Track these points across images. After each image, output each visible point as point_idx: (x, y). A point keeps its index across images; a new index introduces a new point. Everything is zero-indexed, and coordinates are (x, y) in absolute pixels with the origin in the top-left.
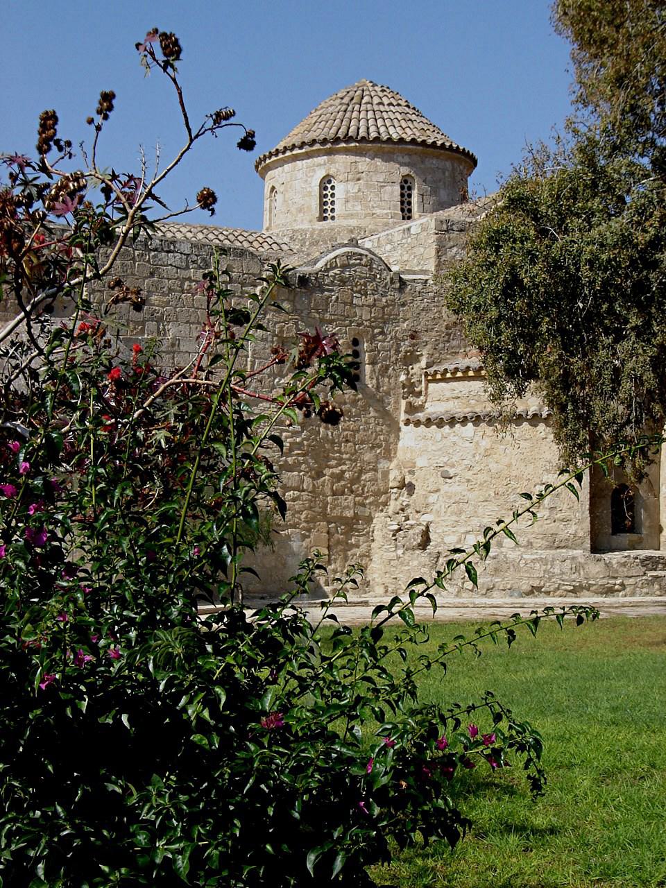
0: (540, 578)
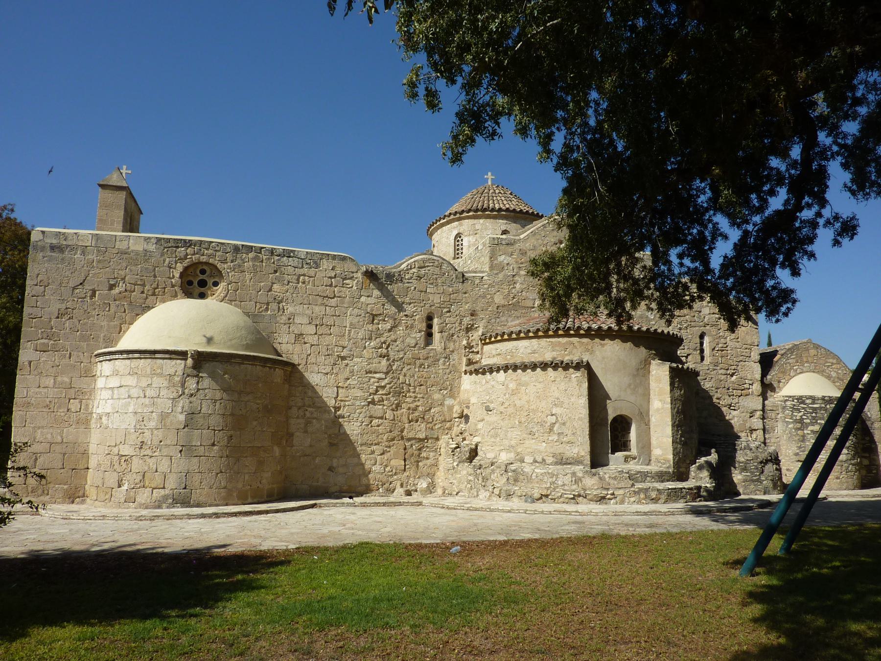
0: (548, 489)
